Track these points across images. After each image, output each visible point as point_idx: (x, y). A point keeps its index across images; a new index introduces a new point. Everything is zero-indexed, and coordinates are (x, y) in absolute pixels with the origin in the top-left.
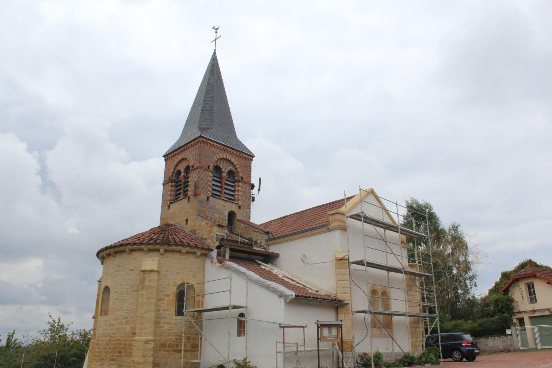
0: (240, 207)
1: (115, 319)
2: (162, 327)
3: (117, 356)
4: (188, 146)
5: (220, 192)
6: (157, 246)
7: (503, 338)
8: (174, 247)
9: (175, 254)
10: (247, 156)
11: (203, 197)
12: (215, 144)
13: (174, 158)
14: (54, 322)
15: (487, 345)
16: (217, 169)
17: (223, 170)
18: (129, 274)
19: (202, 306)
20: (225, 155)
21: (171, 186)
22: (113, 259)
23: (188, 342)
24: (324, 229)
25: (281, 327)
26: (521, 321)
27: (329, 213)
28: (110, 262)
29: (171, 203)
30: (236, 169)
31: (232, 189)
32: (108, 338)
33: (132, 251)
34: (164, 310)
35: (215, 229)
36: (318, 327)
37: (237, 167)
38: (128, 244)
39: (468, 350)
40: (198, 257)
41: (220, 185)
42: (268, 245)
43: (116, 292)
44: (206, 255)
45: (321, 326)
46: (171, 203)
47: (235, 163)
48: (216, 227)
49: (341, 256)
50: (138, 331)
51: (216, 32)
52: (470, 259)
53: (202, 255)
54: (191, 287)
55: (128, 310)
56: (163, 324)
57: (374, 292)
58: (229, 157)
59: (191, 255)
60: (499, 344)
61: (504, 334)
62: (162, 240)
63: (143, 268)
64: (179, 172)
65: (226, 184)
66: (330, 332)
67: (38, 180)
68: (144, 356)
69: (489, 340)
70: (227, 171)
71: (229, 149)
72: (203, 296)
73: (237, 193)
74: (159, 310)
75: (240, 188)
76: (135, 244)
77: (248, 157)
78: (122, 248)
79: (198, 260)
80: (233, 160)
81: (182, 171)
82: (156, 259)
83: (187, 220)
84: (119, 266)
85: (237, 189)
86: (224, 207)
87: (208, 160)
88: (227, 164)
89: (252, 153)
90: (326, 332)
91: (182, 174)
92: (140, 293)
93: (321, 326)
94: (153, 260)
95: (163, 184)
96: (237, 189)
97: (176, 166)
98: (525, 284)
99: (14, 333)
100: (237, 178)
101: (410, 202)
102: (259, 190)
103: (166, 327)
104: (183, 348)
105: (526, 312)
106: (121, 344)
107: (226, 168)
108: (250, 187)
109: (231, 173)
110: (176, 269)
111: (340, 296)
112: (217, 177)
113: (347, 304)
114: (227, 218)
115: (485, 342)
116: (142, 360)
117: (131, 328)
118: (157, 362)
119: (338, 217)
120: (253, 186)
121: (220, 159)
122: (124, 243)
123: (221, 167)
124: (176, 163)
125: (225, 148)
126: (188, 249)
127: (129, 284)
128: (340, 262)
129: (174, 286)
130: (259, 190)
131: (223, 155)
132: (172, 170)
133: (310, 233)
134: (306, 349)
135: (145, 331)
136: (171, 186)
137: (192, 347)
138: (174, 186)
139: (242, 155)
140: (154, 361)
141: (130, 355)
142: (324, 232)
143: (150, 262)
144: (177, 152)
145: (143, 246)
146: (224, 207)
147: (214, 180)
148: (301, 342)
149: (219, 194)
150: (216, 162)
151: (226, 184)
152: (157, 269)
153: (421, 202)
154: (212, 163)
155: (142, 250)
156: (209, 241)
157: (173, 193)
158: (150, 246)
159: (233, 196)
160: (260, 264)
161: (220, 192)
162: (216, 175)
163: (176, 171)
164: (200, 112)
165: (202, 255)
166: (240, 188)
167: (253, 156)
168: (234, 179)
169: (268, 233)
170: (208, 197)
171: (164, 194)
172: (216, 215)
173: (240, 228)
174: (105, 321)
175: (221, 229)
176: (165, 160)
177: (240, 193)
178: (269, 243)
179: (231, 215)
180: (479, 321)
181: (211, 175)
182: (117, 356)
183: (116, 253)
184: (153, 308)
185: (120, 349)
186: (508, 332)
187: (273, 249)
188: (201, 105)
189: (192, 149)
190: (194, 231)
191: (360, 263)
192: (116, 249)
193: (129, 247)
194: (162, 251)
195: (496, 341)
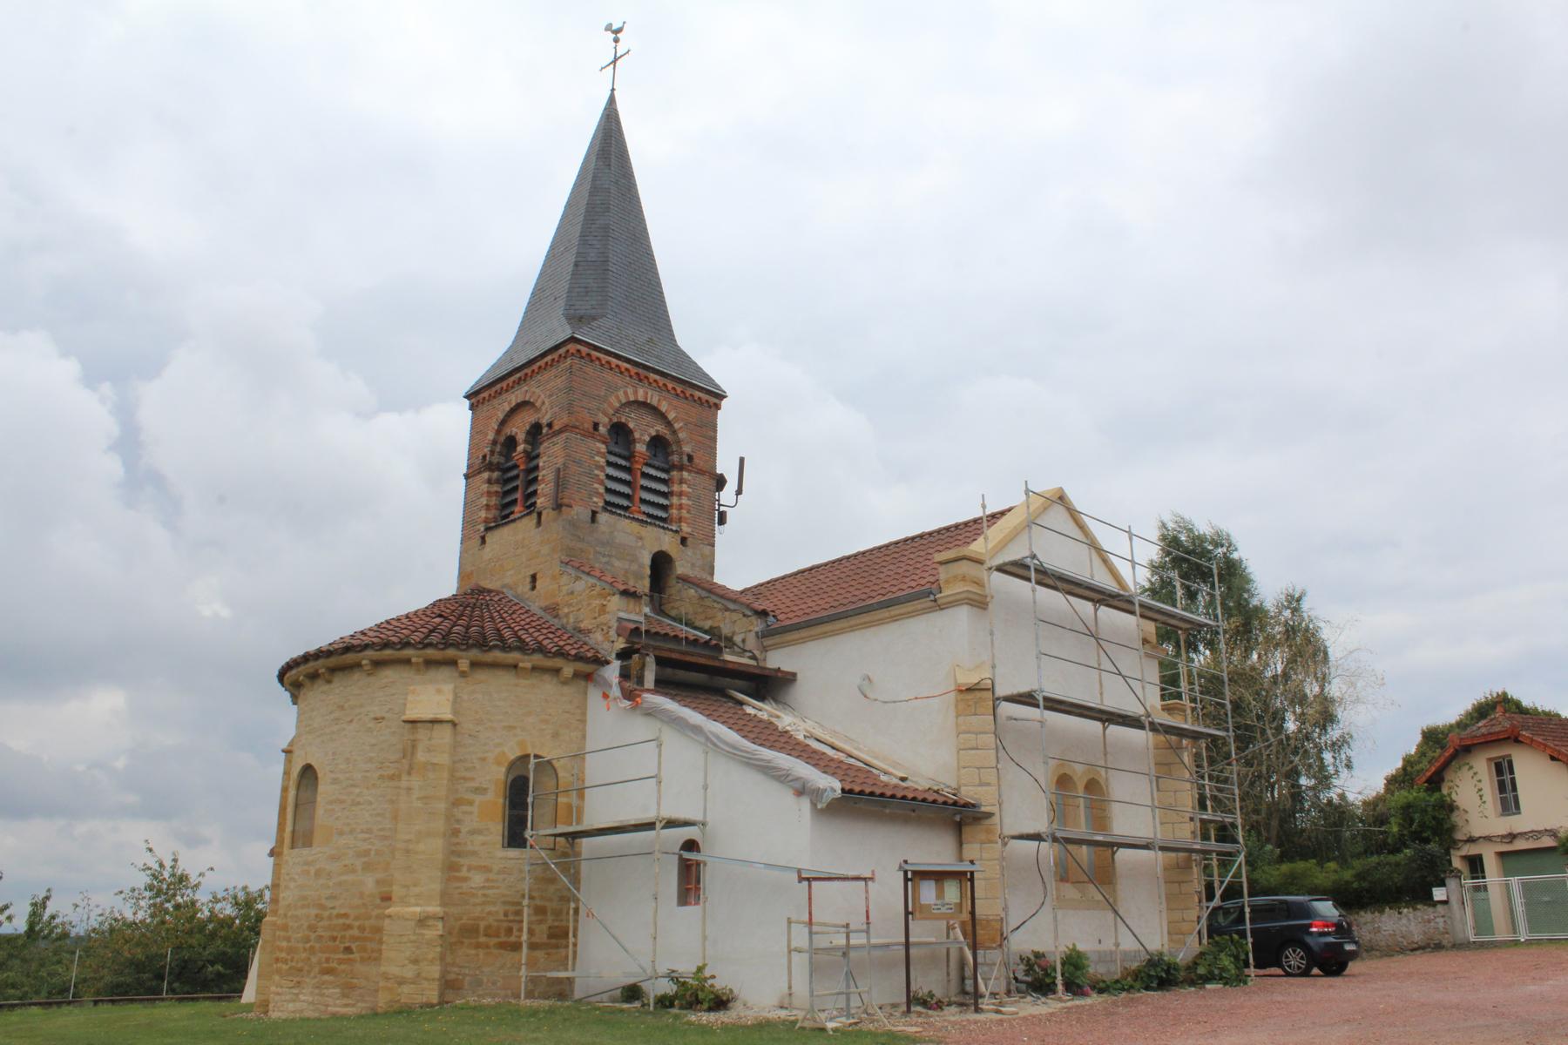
0: (684, 541)
1: (334, 858)
2: (465, 879)
3: (341, 962)
4: (535, 367)
5: (627, 497)
6: (451, 652)
7: (1424, 912)
8: (497, 655)
9: (500, 673)
10: (705, 397)
11: (580, 512)
12: (614, 361)
13: (495, 402)
14: (161, 865)
15: (1378, 930)
16: (620, 432)
17: (637, 435)
18: (370, 730)
19: (579, 821)
20: (641, 392)
21: (489, 481)
22: (326, 687)
23: (540, 922)
24: (926, 603)
25: (801, 879)
26: (1476, 865)
27: (939, 557)
28: (323, 697)
29: (488, 529)
30: (674, 432)
31: (663, 488)
32: (314, 912)
33: (378, 664)
34: (473, 832)
35: (615, 602)
36: (906, 880)
37: (677, 426)
38: (366, 647)
39: (1327, 944)
40: (565, 683)
41: (628, 478)
42: (765, 649)
43: (335, 781)
44: (588, 677)
45: (915, 876)
46: (488, 529)
47: (671, 416)
48: (616, 598)
49: (972, 679)
50: (397, 891)
51: (616, 40)
52: (1335, 689)
53: (577, 675)
54: (546, 766)
55: (369, 831)
56: (470, 869)
57: (1064, 781)
58: (653, 398)
59: (547, 677)
60: (1412, 928)
61: (1428, 899)
62: (461, 633)
63: (411, 714)
64: (511, 442)
65: (645, 475)
66: (940, 894)
67: (114, 466)
68: (415, 961)
69: (1385, 918)
70: (647, 438)
71: (653, 376)
72: (581, 792)
73: (675, 500)
74: (456, 832)
75: (685, 487)
76: (386, 645)
77: (708, 398)
78: (350, 657)
79: (566, 689)
80: (664, 407)
81: (521, 437)
82: (448, 688)
83: (534, 578)
84: (342, 708)
85: (676, 488)
86: (639, 542)
87: (595, 406)
88: (649, 418)
89: (717, 387)
90: (928, 892)
91: (520, 448)
92: (404, 784)
93: (915, 876)
94: (439, 691)
95: (467, 477)
96: (676, 488)
97: (503, 423)
98: (1489, 760)
99: (47, 898)
100: (675, 458)
101: (1171, 525)
102: (739, 492)
103: (477, 879)
104: (525, 937)
105: (1488, 839)
106: (349, 927)
107: (643, 430)
108: (714, 483)
109: (658, 443)
110: (503, 715)
111: (968, 794)
112: (620, 456)
113: (989, 815)
114: (648, 572)
115: (1373, 921)
116: (409, 972)
117: (378, 882)
118: (452, 976)
119: (964, 568)
120: (720, 482)
121: (629, 403)
122: (355, 642)
123: (631, 425)
124: (501, 416)
125: (642, 372)
126: (537, 659)
127: (370, 760)
128: (969, 696)
129: (499, 764)
130: (739, 492)
131: (636, 393)
132: (491, 436)
133: (884, 613)
134: (873, 941)
135: (417, 890)
136: (489, 481)
137: (550, 936)
138: (497, 481)
139: (689, 391)
140: (444, 973)
141: (375, 958)
142: (929, 610)
143: (431, 696)
144: (504, 384)
145: (408, 652)
146: (639, 542)
147: (609, 464)
148: (857, 921)
149: (625, 503)
150: (617, 411)
151: (645, 475)
152: (449, 716)
153: (1203, 528)
154: (605, 414)
155: (408, 662)
156: (598, 636)
157: (494, 501)
158: (430, 652)
159: (664, 508)
160: (741, 703)
161: (627, 497)
162: (617, 450)
163: (502, 439)
164: (571, 268)
165: (577, 675)
166: (685, 487)
167: (722, 397)
168: (667, 462)
169: (763, 614)
170: (594, 513)
171: (467, 504)
172: (617, 563)
173: (684, 600)
174: (307, 863)
175: (632, 602)
176: (472, 407)
177: (685, 501)
178: (767, 642)
179: (661, 563)
180: (1358, 864)
181: (603, 448)
182: (341, 962)
183: (333, 670)
184: (439, 825)
185: (348, 943)
186: (1439, 894)
187: (778, 660)
188: (574, 250)
189: (547, 375)
190: (553, 610)
191: (1027, 699)
192: (333, 661)
193: (369, 653)
194: (464, 664)
195: (1404, 921)
